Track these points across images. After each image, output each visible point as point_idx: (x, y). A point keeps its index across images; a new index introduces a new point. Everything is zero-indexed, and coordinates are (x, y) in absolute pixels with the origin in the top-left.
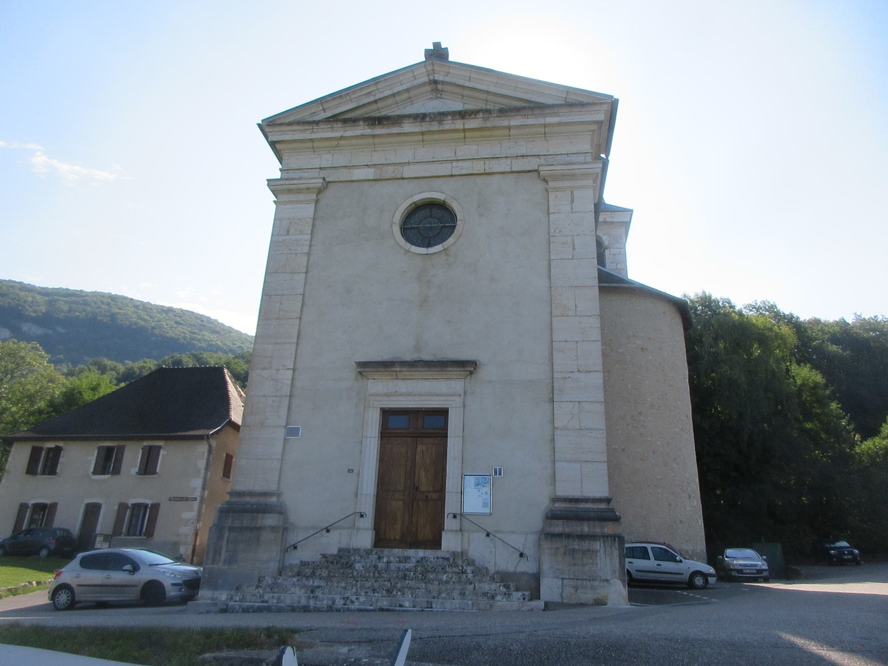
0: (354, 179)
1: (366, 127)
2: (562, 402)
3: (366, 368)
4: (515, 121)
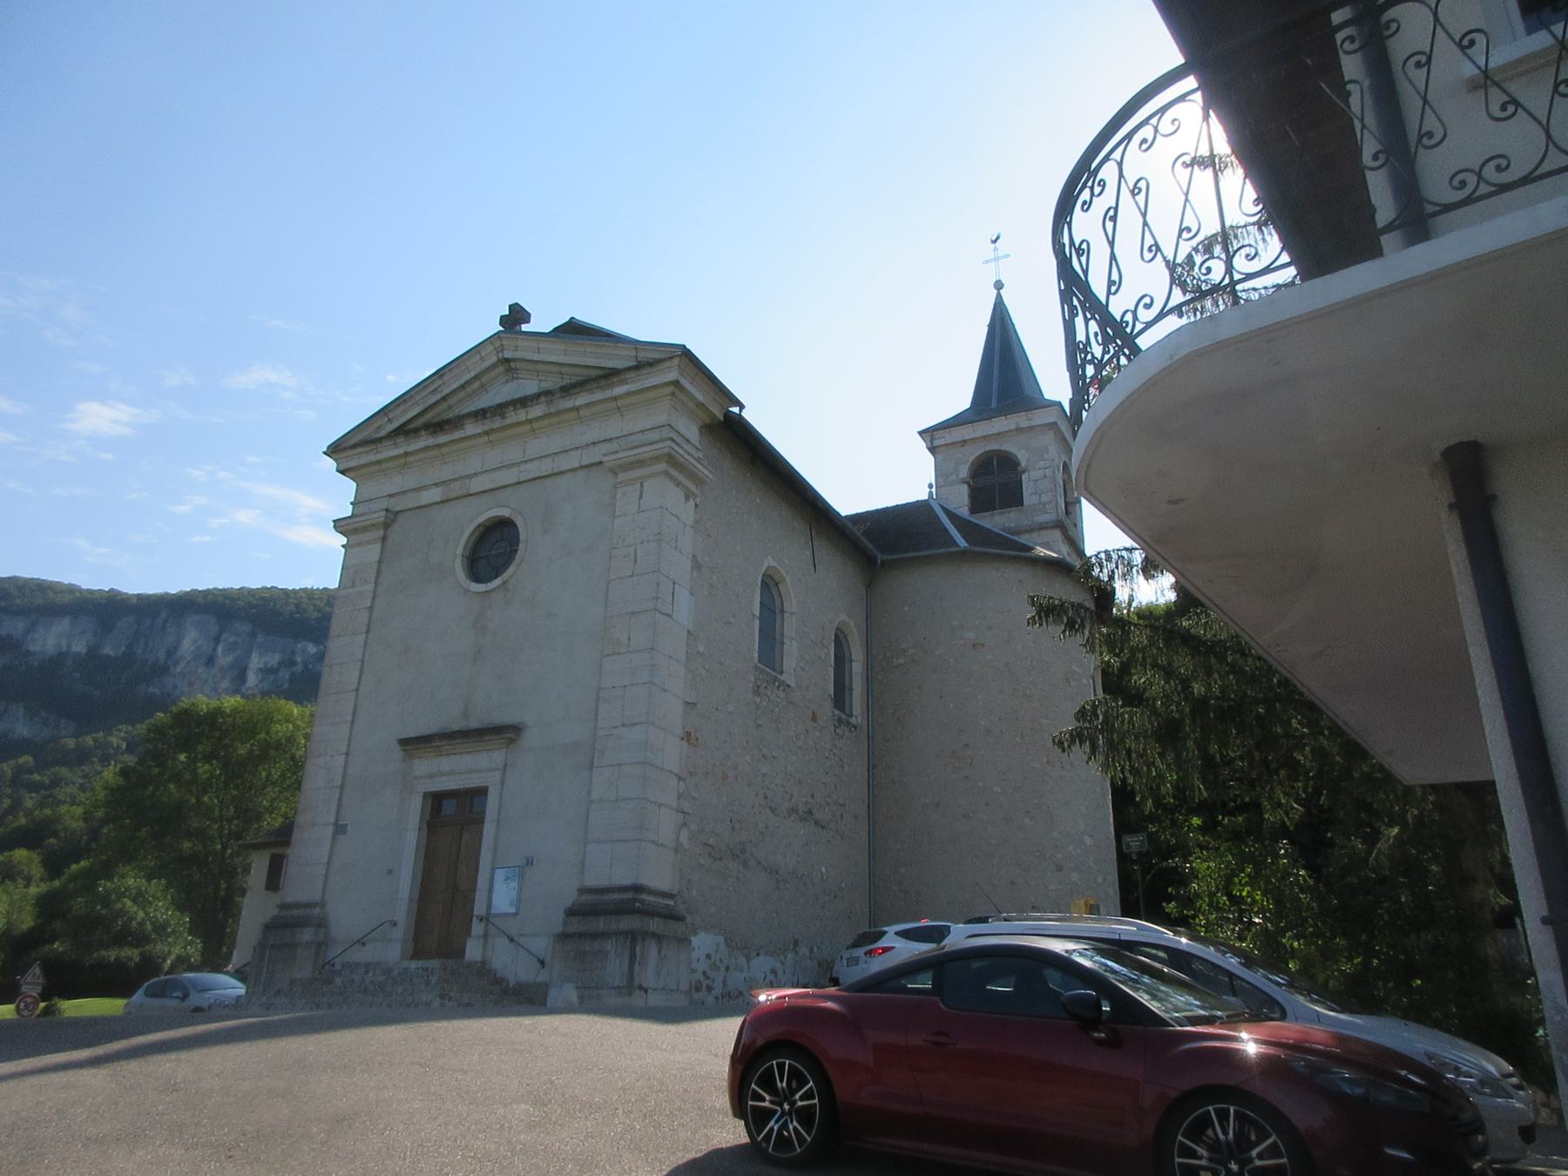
0: (422, 504)
1: (429, 436)
3: (413, 744)
4: (581, 400)
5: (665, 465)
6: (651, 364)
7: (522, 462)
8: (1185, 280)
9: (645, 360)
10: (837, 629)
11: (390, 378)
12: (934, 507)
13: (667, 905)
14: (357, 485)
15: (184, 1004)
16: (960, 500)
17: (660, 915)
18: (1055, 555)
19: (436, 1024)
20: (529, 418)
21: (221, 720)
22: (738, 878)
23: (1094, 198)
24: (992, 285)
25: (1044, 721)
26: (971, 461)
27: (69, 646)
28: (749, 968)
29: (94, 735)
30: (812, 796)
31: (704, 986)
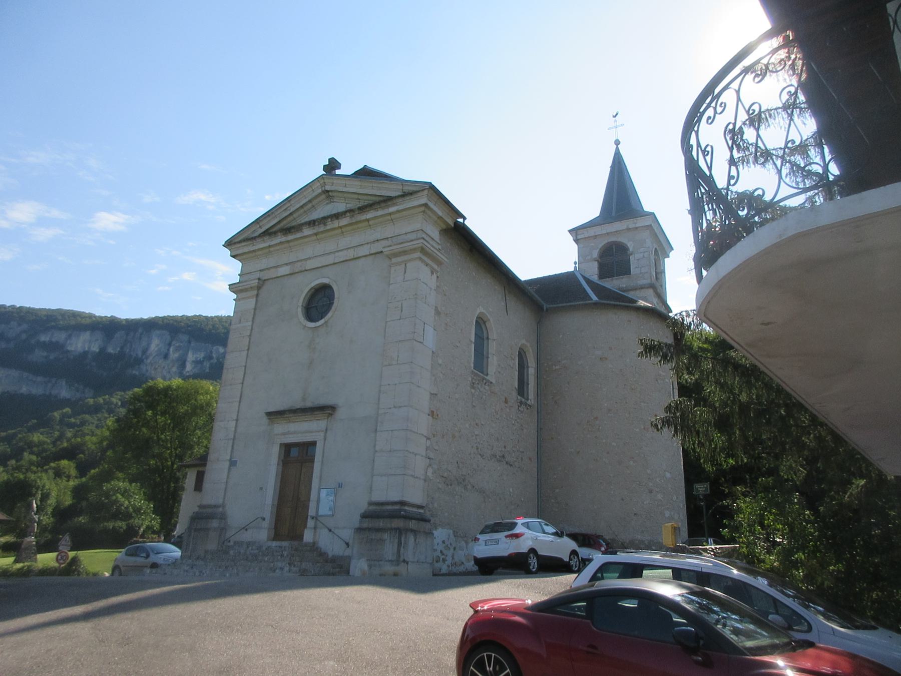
1: (283, 236)
2: (381, 431)
3: (274, 415)
4: (370, 215)
5: (419, 253)
6: (411, 194)
7: (336, 251)
8: (739, 144)
9: (407, 191)
10: (520, 348)
11: (267, 197)
12: (577, 275)
13: (420, 513)
14: (242, 264)
15: (147, 560)
16: (593, 271)
17: (415, 519)
18: (650, 305)
19: (284, 593)
20: (340, 225)
21: (171, 393)
22: (461, 496)
23: (717, 115)
24: (614, 141)
25: (642, 404)
26: (599, 247)
27: (89, 348)
28: (467, 548)
29: (103, 397)
30: (505, 447)
31: (441, 559)
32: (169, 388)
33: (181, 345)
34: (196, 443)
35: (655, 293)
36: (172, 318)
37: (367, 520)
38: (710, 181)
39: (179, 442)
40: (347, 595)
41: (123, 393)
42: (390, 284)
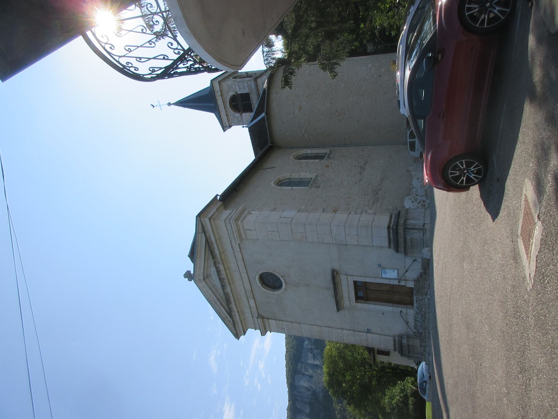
3: (339, 307)
4: (217, 252)
16: (248, 116)
23: (133, 66)
24: (169, 107)
25: (327, 83)
28: (416, 188)
31: (423, 203)
32: (328, 373)
33: (304, 367)
34: (362, 356)
35: (260, 77)
36: (287, 374)
37: (399, 249)
38: (167, 68)
39: (361, 367)
40: (437, 259)
41: (334, 403)
42: (258, 239)
